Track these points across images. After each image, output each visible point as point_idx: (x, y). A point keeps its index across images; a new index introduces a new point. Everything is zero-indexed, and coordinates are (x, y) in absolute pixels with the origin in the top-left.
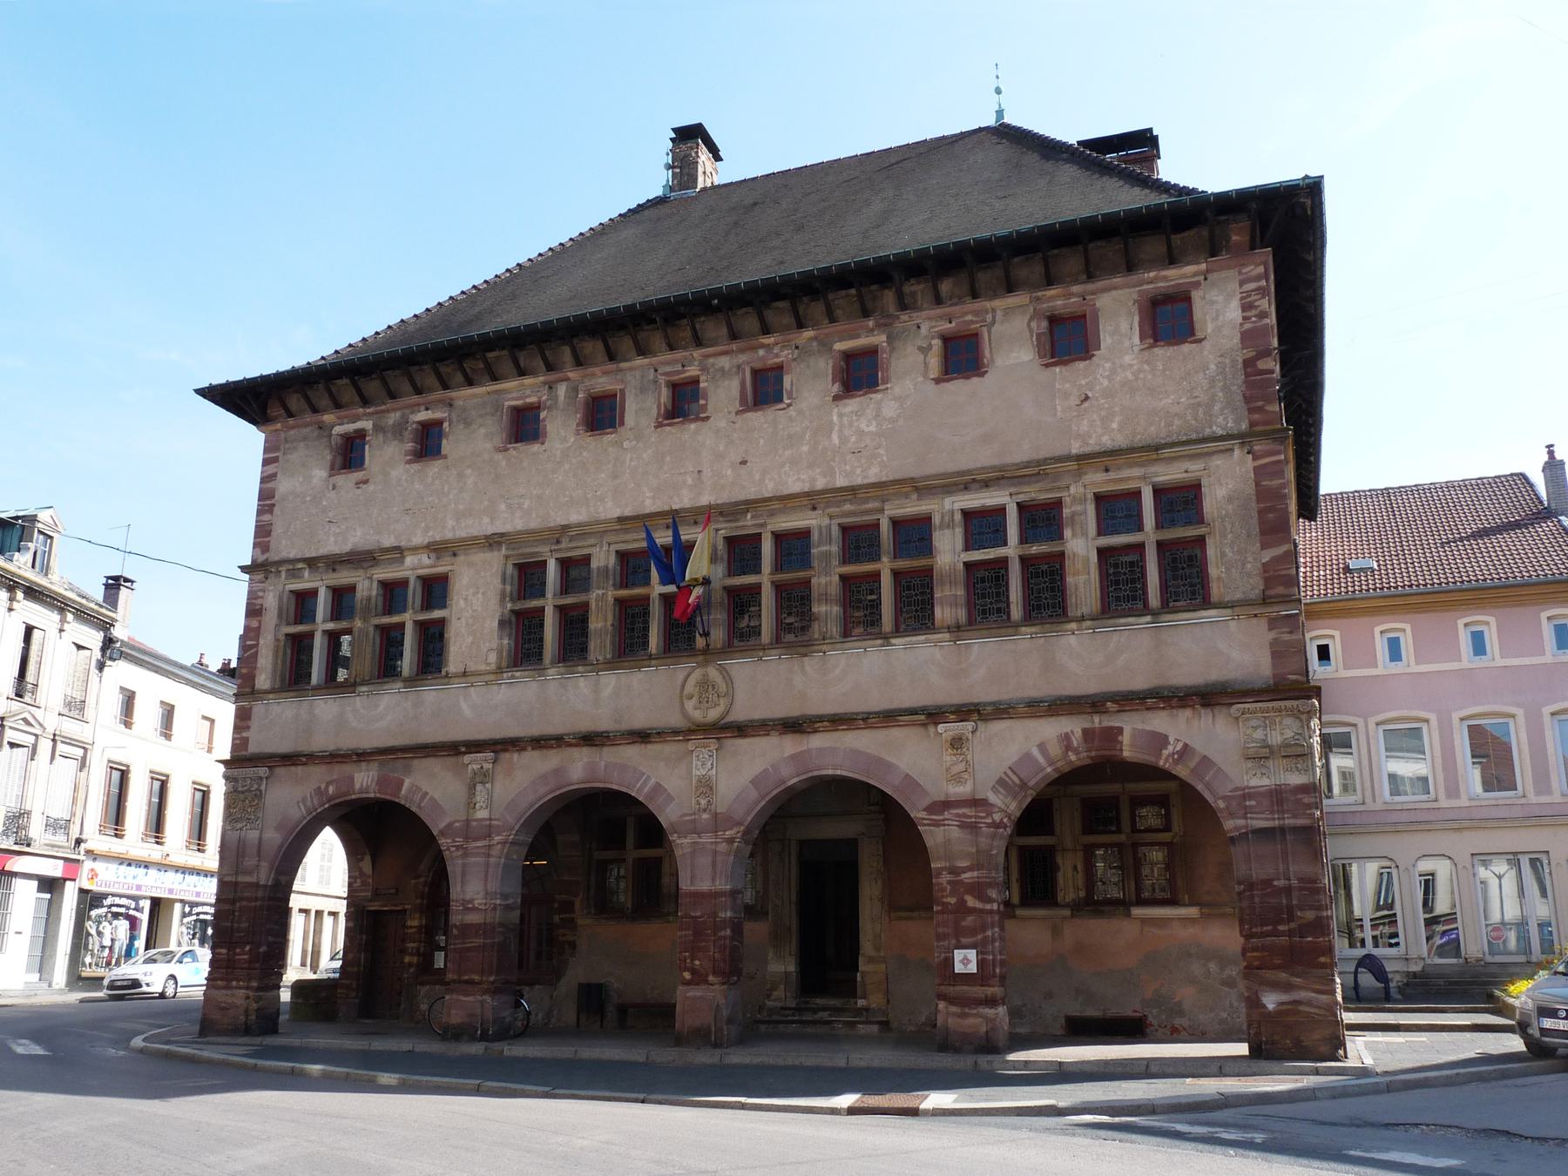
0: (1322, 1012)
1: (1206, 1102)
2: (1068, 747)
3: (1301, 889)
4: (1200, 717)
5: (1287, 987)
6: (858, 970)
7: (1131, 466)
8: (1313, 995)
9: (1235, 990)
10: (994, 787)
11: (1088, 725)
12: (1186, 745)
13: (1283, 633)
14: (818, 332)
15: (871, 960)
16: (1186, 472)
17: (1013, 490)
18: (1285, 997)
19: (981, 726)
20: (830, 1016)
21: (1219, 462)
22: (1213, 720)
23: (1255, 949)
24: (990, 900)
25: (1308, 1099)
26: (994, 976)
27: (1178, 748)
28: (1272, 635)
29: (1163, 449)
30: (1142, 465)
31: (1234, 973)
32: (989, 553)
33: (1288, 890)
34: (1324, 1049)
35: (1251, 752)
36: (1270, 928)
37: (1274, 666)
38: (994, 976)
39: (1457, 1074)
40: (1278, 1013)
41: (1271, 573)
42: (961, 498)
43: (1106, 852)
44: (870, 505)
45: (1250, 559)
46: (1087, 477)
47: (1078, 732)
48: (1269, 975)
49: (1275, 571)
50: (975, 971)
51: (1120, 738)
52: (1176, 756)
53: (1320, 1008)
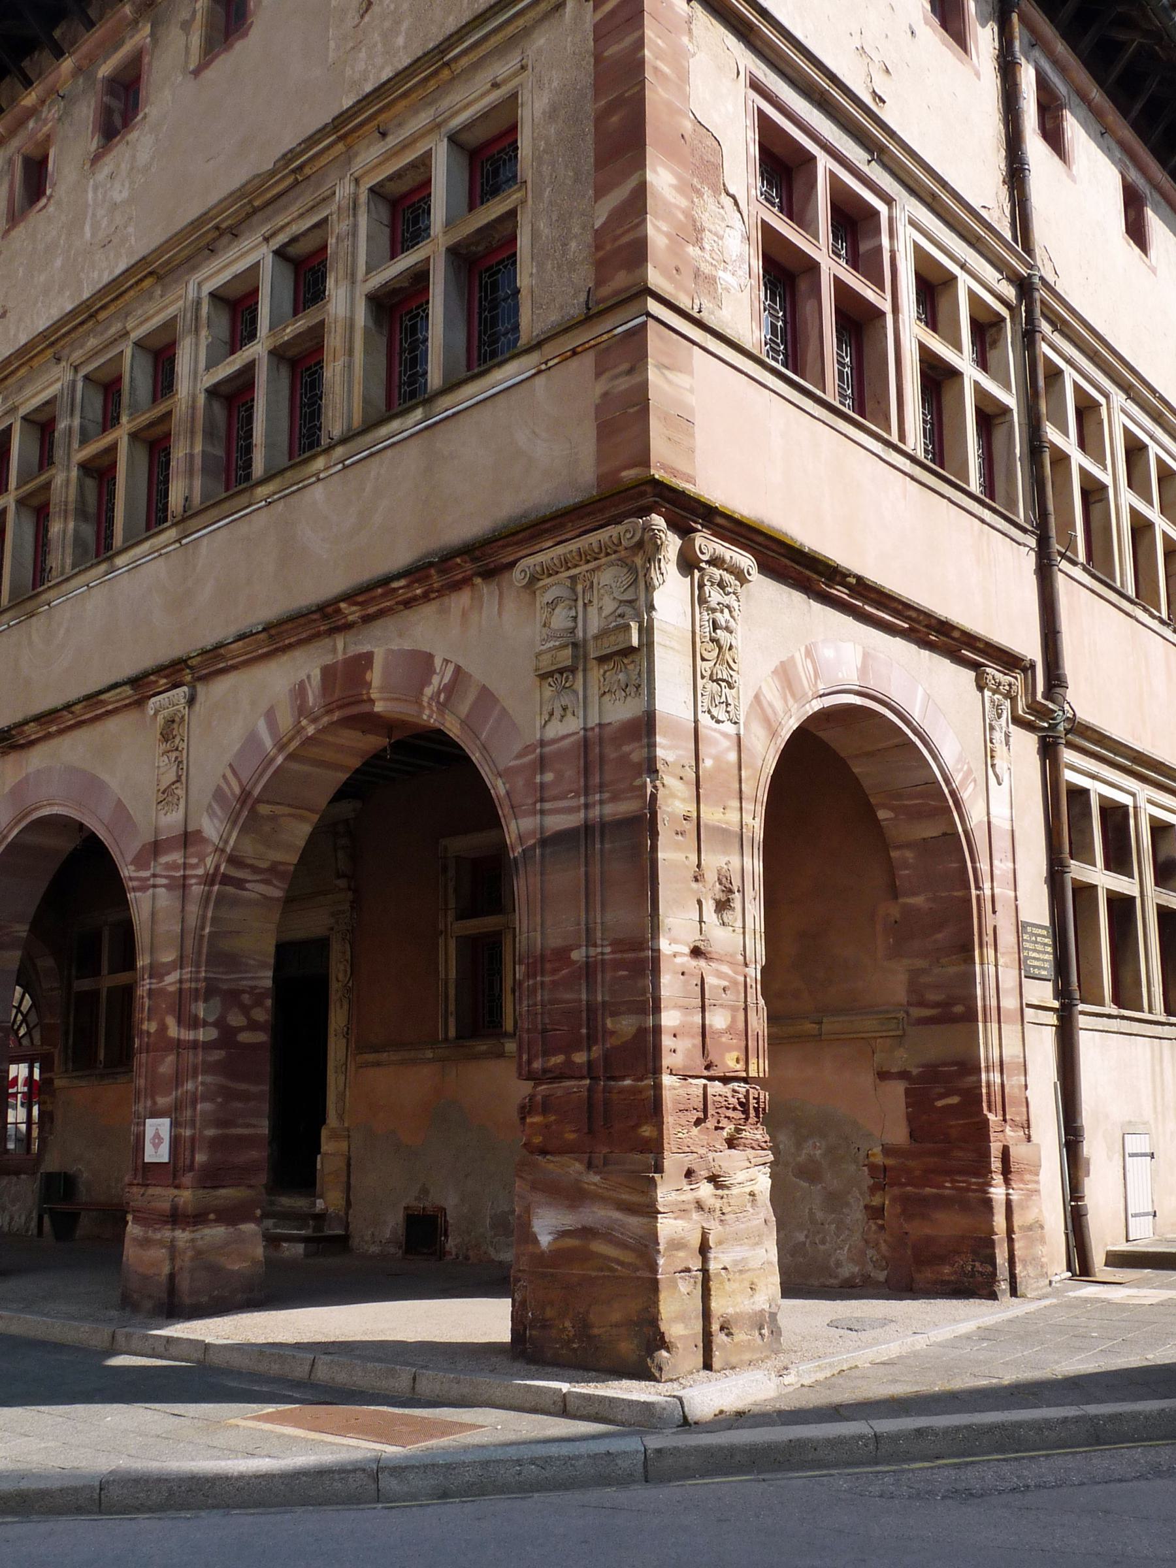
0: (628, 1257)
1: (43, 1494)
2: (302, 710)
3: (618, 965)
4: (481, 608)
5: (574, 1196)
6: (319, 1153)
7: (414, 110)
8: (617, 1215)
9: (819, 1187)
10: (210, 805)
11: (328, 660)
12: (458, 669)
13: (616, 377)
14: (78, 55)
15: (334, 1135)
16: (495, 85)
17: (265, 229)
18: (568, 1220)
19: (201, 688)
20: (276, 1226)
21: (542, 41)
22: (500, 604)
23: (546, 1107)
24: (195, 1023)
25: (353, 1500)
26: (191, 1168)
27: (446, 680)
28: (600, 388)
29: (451, 47)
30: (428, 101)
31: (818, 1152)
32: (234, 361)
33: (589, 970)
34: (627, 1348)
35: (546, 664)
36: (559, 1059)
37: (601, 458)
38: (191, 1168)
39: (920, 1432)
40: (558, 1257)
41: (608, 247)
42: (197, 276)
43: (1027, 933)
44: (112, 331)
45: (576, 230)
46: (359, 159)
47: (316, 674)
48: (552, 1166)
49: (616, 238)
50: (166, 1160)
51: (368, 677)
52: (442, 696)
53: (624, 1246)
